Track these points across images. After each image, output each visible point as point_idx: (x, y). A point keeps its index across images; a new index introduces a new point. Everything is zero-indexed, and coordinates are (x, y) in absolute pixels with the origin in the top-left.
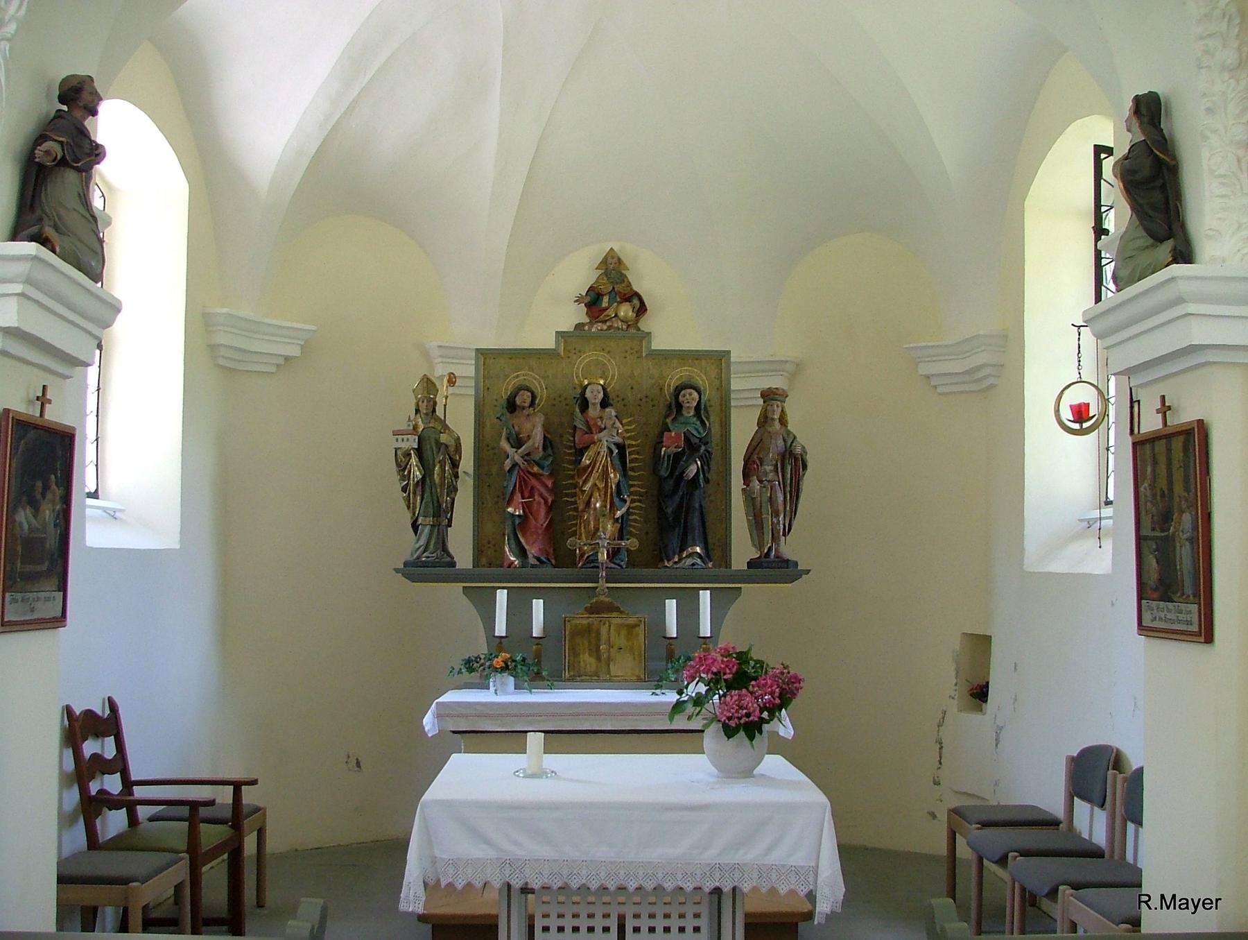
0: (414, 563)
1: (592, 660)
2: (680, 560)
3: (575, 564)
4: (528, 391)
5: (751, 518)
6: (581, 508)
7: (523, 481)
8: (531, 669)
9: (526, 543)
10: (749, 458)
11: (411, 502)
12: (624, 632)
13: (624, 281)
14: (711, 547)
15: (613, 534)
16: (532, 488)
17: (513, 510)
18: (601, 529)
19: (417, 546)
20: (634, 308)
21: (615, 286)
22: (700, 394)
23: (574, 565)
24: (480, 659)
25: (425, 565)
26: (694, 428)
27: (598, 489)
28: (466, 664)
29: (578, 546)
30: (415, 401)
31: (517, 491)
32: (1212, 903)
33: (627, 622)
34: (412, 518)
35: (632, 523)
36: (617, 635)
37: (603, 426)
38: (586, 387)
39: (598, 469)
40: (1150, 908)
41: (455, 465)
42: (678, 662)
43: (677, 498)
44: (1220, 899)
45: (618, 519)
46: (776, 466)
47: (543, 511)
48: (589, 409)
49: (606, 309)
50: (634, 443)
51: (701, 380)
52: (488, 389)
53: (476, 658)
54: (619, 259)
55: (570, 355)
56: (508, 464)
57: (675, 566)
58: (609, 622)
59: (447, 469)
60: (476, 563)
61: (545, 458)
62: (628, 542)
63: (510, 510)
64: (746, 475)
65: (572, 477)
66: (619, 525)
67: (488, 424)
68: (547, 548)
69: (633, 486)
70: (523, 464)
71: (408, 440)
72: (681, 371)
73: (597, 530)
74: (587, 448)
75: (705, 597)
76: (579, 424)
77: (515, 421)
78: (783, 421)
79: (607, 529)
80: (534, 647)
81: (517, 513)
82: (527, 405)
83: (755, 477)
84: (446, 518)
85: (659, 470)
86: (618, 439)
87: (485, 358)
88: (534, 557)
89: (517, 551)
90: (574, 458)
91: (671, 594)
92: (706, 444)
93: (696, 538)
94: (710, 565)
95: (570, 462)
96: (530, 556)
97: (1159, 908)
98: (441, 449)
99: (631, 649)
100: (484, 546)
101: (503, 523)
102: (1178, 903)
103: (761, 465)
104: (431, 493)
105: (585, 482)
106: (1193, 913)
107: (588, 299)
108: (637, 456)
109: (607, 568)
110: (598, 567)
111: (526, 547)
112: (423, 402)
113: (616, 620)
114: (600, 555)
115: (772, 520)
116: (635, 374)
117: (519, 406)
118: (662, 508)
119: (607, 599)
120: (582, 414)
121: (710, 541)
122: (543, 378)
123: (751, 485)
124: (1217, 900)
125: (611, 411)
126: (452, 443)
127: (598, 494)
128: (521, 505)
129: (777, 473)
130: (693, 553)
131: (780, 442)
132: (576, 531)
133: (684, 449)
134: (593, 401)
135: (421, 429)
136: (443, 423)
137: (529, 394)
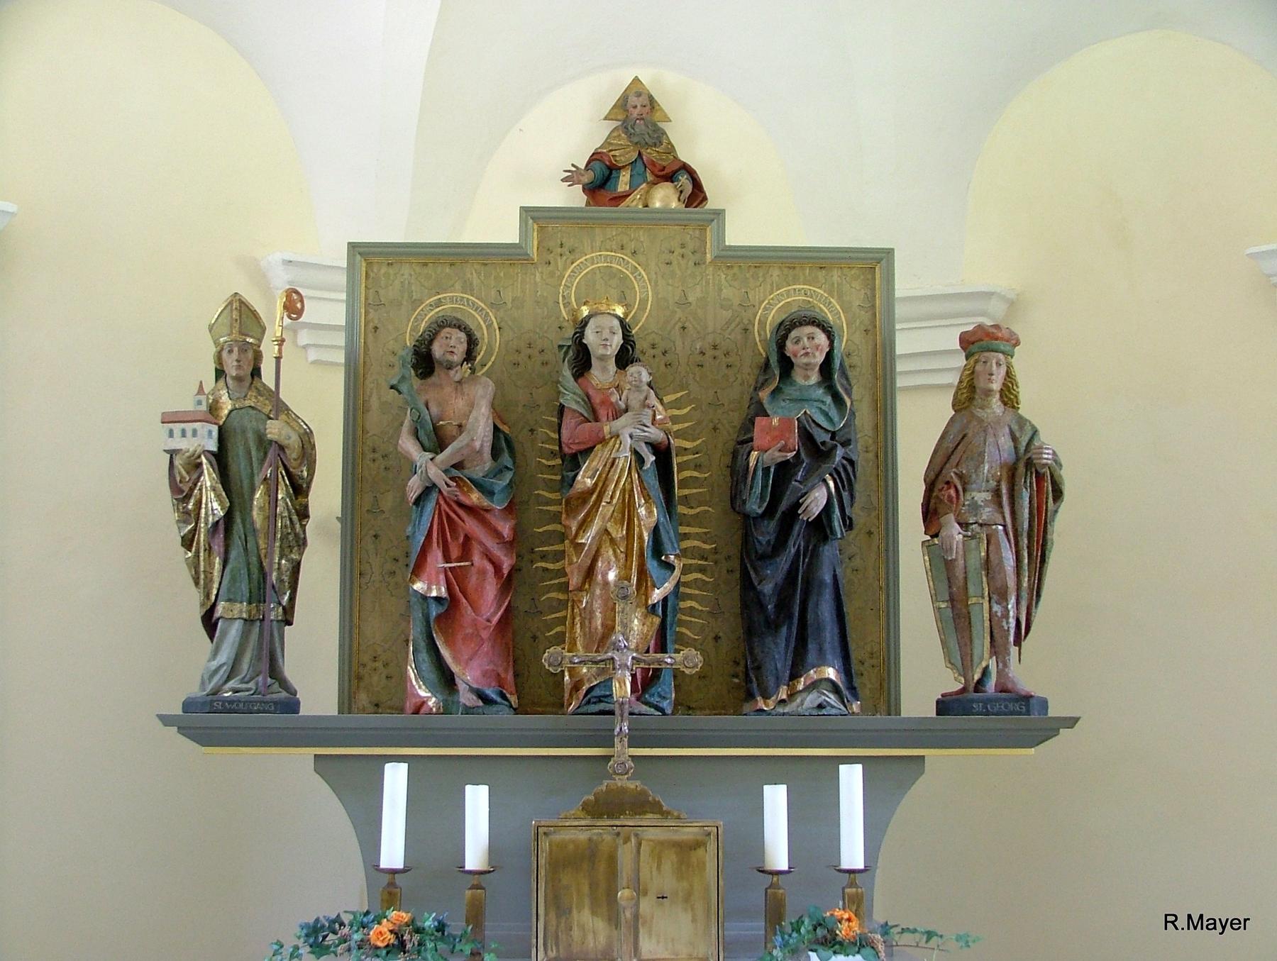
0: (204, 703)
1: (600, 925)
2: (792, 696)
3: (562, 705)
4: (459, 328)
5: (943, 605)
6: (575, 580)
7: (447, 526)
8: (458, 947)
9: (454, 658)
10: (937, 476)
11: (202, 569)
12: (670, 859)
13: (661, 143)
14: (855, 667)
15: (644, 637)
16: (467, 538)
17: (425, 587)
18: (618, 628)
19: (214, 664)
20: (681, 192)
21: (642, 151)
22: (830, 336)
23: (559, 707)
24: (342, 924)
25: (230, 707)
26: (819, 409)
27: (612, 541)
28: (307, 935)
29: (567, 664)
30: (213, 350)
31: (435, 545)
32: (1240, 923)
33: (676, 837)
34: (202, 605)
35: (684, 618)
36: (654, 869)
37: (623, 406)
38: (584, 323)
39: (612, 498)
40: (1177, 929)
41: (299, 489)
42: (798, 931)
43: (784, 562)
44: (1249, 919)
45: (654, 605)
46: (997, 493)
47: (491, 589)
48: (592, 371)
49: (625, 196)
50: (688, 445)
51: (831, 312)
52: (376, 328)
53: (334, 921)
54: (651, 99)
55: (551, 258)
56: (414, 486)
57: (780, 710)
58: (636, 835)
59: (280, 497)
60: (347, 702)
61: (498, 472)
62: (679, 657)
63: (419, 586)
64: (931, 513)
65: (556, 518)
66: (657, 621)
67: (374, 403)
68: (500, 670)
69: (686, 536)
70: (448, 486)
71: (195, 433)
72: (788, 294)
73: (609, 629)
74: (588, 451)
75: (851, 779)
76: (571, 401)
77: (432, 395)
78: (1009, 396)
79: (632, 629)
80: (468, 893)
81: (434, 594)
82: (457, 358)
83: (951, 517)
84: (280, 604)
85: (744, 502)
86: (656, 434)
87: (369, 264)
88: (472, 690)
89: (433, 676)
90: (559, 477)
91: (776, 770)
92: (846, 444)
93: (827, 646)
94: (856, 706)
95: (549, 486)
96: (462, 687)
97: (1186, 928)
98: (269, 456)
99: (688, 898)
100: (364, 665)
101: (406, 617)
102: (1205, 923)
103: (964, 490)
104: (246, 549)
105: (584, 526)
106: (1220, 934)
107: (588, 178)
108: (696, 474)
109: (631, 714)
110: (611, 713)
111: (455, 668)
112: (230, 351)
113: (653, 831)
114: (616, 685)
115: (990, 608)
116: (690, 299)
117: (440, 363)
118: (751, 583)
119: (631, 785)
120: (576, 380)
121: (855, 655)
122: (492, 305)
123: (943, 533)
124: (1245, 920)
125: (640, 373)
126: (293, 441)
127: (611, 552)
128: (442, 577)
129: (1000, 505)
130: (821, 680)
131: (1005, 442)
132: (564, 633)
133: (798, 455)
134: (601, 351)
135: (226, 412)
136: (274, 396)
137: (463, 336)
